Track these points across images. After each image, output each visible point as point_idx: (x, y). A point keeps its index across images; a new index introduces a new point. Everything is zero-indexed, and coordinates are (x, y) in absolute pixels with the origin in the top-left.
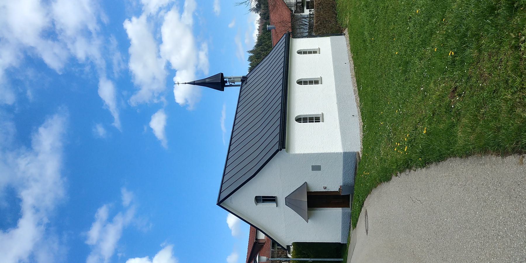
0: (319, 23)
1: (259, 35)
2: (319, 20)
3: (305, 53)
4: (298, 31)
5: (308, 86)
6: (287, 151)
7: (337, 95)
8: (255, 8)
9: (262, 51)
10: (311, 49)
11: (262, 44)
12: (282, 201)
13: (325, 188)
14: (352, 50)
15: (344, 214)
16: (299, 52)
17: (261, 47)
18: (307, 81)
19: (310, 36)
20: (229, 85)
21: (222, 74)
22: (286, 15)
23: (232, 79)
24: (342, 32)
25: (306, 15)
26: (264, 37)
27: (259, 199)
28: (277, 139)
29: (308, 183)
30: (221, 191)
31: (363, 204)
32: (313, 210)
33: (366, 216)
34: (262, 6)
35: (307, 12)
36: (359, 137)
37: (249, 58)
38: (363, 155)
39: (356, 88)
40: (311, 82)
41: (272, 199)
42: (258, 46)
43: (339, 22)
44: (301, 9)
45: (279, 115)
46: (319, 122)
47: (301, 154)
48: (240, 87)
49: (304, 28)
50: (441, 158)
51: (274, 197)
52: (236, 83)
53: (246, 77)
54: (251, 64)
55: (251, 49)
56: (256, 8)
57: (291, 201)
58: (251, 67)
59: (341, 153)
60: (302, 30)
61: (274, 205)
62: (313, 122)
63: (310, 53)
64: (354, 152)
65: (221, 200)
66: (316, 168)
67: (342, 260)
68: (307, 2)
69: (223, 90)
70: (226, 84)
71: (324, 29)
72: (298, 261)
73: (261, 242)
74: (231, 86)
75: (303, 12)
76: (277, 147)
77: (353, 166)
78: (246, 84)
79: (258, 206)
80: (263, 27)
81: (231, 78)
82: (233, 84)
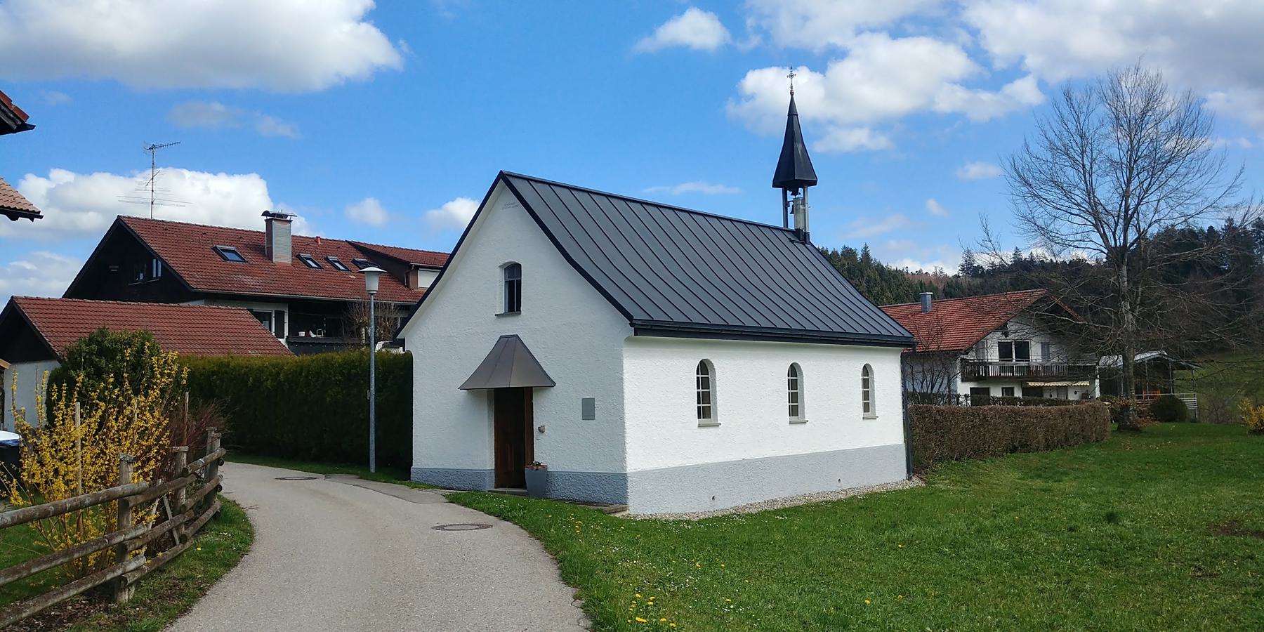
1: (907, 273)
5: (785, 391)
6: (628, 340)
7: (763, 460)
9: (868, 282)
11: (886, 282)
12: (511, 326)
13: (541, 430)
15: (479, 474)
19: (907, 396)
20: (788, 200)
21: (814, 183)
22: (955, 339)
23: (801, 207)
24: (914, 472)
26: (901, 284)
28: (658, 316)
32: (489, 401)
33: (477, 527)
34: (978, 281)
35: (963, 388)
37: (851, 249)
38: (621, 521)
39: (779, 506)
40: (794, 398)
41: (514, 304)
43: (939, 467)
45: (715, 320)
46: (699, 417)
47: (622, 374)
48: (781, 225)
51: (519, 309)
52: (791, 217)
53: (805, 239)
55: (872, 255)
56: (975, 265)
57: (510, 349)
58: (830, 253)
59: (624, 468)
60: (920, 376)
61: (501, 309)
62: (699, 403)
63: (866, 395)
64: (626, 498)
66: (588, 409)
68: (989, 388)
70: (789, 193)
71: (922, 429)
73: (411, 279)
74: (786, 204)
75: (963, 380)
76: (638, 315)
79: (498, 270)
80: (927, 284)
81: (804, 204)
82: (790, 209)
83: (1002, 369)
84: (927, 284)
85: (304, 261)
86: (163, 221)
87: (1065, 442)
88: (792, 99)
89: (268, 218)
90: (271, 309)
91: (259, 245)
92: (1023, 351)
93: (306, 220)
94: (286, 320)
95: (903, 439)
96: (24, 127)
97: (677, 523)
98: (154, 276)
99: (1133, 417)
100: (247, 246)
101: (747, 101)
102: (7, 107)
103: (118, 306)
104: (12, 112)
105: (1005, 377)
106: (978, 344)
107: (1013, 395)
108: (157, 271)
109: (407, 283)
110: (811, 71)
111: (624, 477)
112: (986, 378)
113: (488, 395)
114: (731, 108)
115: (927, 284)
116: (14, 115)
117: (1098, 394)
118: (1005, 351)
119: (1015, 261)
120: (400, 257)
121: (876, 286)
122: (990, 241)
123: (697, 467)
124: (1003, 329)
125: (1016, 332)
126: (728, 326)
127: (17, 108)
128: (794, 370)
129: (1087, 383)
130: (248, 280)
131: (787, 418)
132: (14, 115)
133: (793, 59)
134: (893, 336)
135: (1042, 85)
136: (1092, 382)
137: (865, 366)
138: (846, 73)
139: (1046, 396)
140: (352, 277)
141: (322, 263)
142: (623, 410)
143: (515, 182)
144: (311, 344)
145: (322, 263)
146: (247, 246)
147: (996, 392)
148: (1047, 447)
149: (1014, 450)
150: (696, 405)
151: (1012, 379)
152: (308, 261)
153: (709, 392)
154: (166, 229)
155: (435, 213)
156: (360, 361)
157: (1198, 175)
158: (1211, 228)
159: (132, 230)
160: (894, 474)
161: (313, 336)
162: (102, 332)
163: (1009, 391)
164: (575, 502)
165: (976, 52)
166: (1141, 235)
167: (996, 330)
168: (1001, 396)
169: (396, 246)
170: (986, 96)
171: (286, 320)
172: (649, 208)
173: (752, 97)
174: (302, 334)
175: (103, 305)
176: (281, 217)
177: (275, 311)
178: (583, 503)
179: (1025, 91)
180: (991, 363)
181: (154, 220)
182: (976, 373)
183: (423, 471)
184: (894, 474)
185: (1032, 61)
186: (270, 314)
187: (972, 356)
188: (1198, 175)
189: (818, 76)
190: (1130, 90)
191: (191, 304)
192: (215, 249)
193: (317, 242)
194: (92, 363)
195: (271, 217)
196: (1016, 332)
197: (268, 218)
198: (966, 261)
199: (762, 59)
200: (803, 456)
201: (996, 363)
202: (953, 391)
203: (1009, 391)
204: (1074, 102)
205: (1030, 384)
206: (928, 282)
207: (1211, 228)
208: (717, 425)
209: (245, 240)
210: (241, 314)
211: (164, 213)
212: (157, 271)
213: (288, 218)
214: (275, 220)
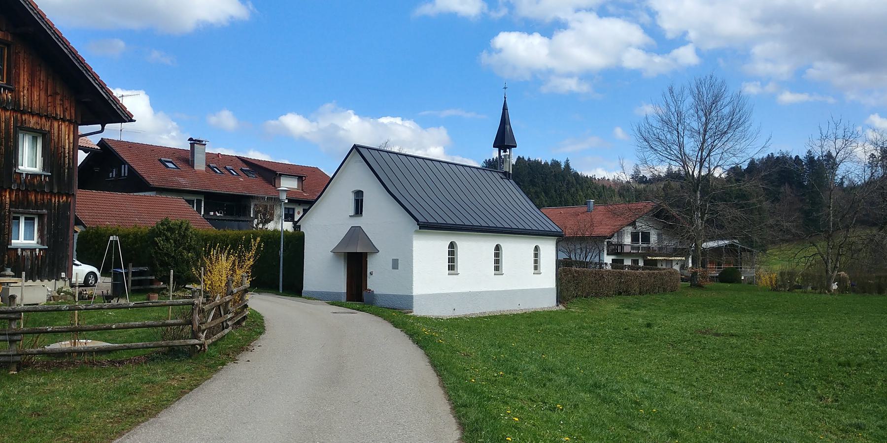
0: (575, 274)
1: (595, 179)
2: (579, 275)
3: (536, 255)
4: (578, 246)
5: (492, 258)
6: (416, 231)
7: (480, 292)
8: (639, 174)
9: (568, 184)
10: (540, 263)
11: (579, 184)
12: (357, 222)
13: (371, 274)
14: (535, 312)
15: (339, 294)
16: (537, 248)
17: (575, 182)
18: (499, 257)
19: (559, 263)
21: (516, 147)
22: (600, 231)
23: (508, 160)
24: (561, 303)
25: (604, 258)
26: (590, 187)
27: (359, 196)
28: (431, 220)
29: (377, 254)
30: (370, 149)
31: (361, 311)
32: (345, 259)
34: (643, 186)
35: (608, 259)
36: (430, 315)
37: (557, 161)
38: (411, 316)
39: (487, 315)
40: (497, 262)
41: (359, 209)
42: (576, 175)
43: (575, 300)
44: (613, 250)
45: (459, 222)
46: (449, 270)
47: (412, 248)
49: (582, 255)
50: (421, 347)
51: (361, 213)
54: (546, 164)
55: (572, 166)
56: (641, 175)
57: (356, 233)
58: (543, 163)
59: (412, 293)
60: (579, 251)
61: (352, 213)
62: (449, 263)
63: (536, 262)
64: (412, 307)
65: (359, 148)
66: (395, 264)
67: (281, 292)
68: (623, 260)
69: (494, 147)
70: (502, 151)
71: (566, 280)
72: (280, 238)
73: (277, 181)
75: (608, 254)
76: (421, 219)
77: (396, 306)
78: (501, 178)
79: (351, 193)
80: (608, 186)
81: (509, 158)
83: (633, 248)
84: (608, 187)
85: (212, 168)
86: (128, 142)
87: (648, 292)
88: (505, 101)
89: (192, 142)
90: (194, 198)
91: (185, 159)
92: (646, 237)
93: (177, 124)
94: (203, 205)
95: (555, 285)
96: (132, 121)
97: (437, 319)
98: (123, 175)
99: (699, 279)
100: (178, 159)
101: (497, 53)
102: (124, 111)
103: (111, 195)
104: (127, 114)
105: (633, 253)
106: (619, 233)
107: (638, 264)
108: (124, 171)
109: (274, 184)
110: (542, 36)
111: (411, 297)
112: (621, 254)
113: (344, 255)
114: (484, 57)
115: (608, 187)
116: (128, 115)
117: (690, 265)
118: (635, 238)
119: (668, 173)
120: (264, 166)
121: (573, 187)
122: (624, 173)
123: (447, 294)
124: (633, 224)
125: (641, 226)
126: (465, 225)
127: (129, 112)
128: (498, 248)
129: (684, 258)
130: (181, 180)
131: (493, 272)
132: (128, 115)
133: (528, 26)
134: (557, 231)
135: (698, 52)
136: (687, 259)
137: (536, 247)
138: (563, 38)
139: (659, 266)
140: (241, 179)
141: (223, 171)
142: (412, 265)
143: (361, 150)
144: (217, 219)
145: (223, 171)
146: (178, 159)
147: (628, 262)
148: (640, 293)
149: (620, 294)
150: (448, 264)
151: (638, 254)
152: (215, 169)
153: (499, 253)
154: (130, 147)
155: (273, 122)
156: (273, 235)
157: (744, 140)
158: (797, 157)
159: (111, 147)
160: (549, 302)
161: (218, 215)
162: (166, 219)
163: (635, 262)
164: (389, 308)
165: (653, 30)
166: (710, 174)
167: (629, 225)
168: (631, 264)
169: (266, 160)
170: (657, 59)
171: (203, 205)
172: (427, 161)
173: (500, 51)
174: (212, 213)
175: (103, 194)
176: (199, 142)
177: (197, 199)
178: (392, 309)
179: (686, 55)
180: (625, 245)
181: (122, 141)
182: (616, 250)
183: (308, 292)
184: (549, 302)
185: (692, 35)
186: (193, 201)
187: (614, 240)
188: (744, 140)
189: (545, 40)
190: (707, 89)
191: (141, 194)
192: (160, 160)
193: (218, 156)
194: (164, 234)
195: (194, 142)
196: (641, 226)
197: (192, 142)
198: (635, 172)
199: (509, 25)
200: (500, 291)
201: (628, 245)
202: (602, 260)
203: (635, 262)
204: (674, 94)
205: (648, 258)
206: (609, 186)
207: (797, 157)
208: (458, 274)
209: (177, 155)
210: (180, 201)
211: (125, 138)
212: (124, 171)
213: (204, 143)
214: (196, 144)
